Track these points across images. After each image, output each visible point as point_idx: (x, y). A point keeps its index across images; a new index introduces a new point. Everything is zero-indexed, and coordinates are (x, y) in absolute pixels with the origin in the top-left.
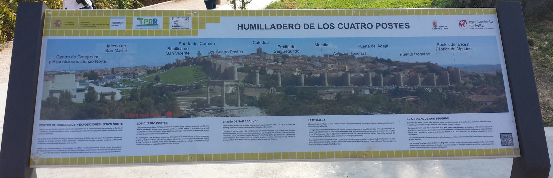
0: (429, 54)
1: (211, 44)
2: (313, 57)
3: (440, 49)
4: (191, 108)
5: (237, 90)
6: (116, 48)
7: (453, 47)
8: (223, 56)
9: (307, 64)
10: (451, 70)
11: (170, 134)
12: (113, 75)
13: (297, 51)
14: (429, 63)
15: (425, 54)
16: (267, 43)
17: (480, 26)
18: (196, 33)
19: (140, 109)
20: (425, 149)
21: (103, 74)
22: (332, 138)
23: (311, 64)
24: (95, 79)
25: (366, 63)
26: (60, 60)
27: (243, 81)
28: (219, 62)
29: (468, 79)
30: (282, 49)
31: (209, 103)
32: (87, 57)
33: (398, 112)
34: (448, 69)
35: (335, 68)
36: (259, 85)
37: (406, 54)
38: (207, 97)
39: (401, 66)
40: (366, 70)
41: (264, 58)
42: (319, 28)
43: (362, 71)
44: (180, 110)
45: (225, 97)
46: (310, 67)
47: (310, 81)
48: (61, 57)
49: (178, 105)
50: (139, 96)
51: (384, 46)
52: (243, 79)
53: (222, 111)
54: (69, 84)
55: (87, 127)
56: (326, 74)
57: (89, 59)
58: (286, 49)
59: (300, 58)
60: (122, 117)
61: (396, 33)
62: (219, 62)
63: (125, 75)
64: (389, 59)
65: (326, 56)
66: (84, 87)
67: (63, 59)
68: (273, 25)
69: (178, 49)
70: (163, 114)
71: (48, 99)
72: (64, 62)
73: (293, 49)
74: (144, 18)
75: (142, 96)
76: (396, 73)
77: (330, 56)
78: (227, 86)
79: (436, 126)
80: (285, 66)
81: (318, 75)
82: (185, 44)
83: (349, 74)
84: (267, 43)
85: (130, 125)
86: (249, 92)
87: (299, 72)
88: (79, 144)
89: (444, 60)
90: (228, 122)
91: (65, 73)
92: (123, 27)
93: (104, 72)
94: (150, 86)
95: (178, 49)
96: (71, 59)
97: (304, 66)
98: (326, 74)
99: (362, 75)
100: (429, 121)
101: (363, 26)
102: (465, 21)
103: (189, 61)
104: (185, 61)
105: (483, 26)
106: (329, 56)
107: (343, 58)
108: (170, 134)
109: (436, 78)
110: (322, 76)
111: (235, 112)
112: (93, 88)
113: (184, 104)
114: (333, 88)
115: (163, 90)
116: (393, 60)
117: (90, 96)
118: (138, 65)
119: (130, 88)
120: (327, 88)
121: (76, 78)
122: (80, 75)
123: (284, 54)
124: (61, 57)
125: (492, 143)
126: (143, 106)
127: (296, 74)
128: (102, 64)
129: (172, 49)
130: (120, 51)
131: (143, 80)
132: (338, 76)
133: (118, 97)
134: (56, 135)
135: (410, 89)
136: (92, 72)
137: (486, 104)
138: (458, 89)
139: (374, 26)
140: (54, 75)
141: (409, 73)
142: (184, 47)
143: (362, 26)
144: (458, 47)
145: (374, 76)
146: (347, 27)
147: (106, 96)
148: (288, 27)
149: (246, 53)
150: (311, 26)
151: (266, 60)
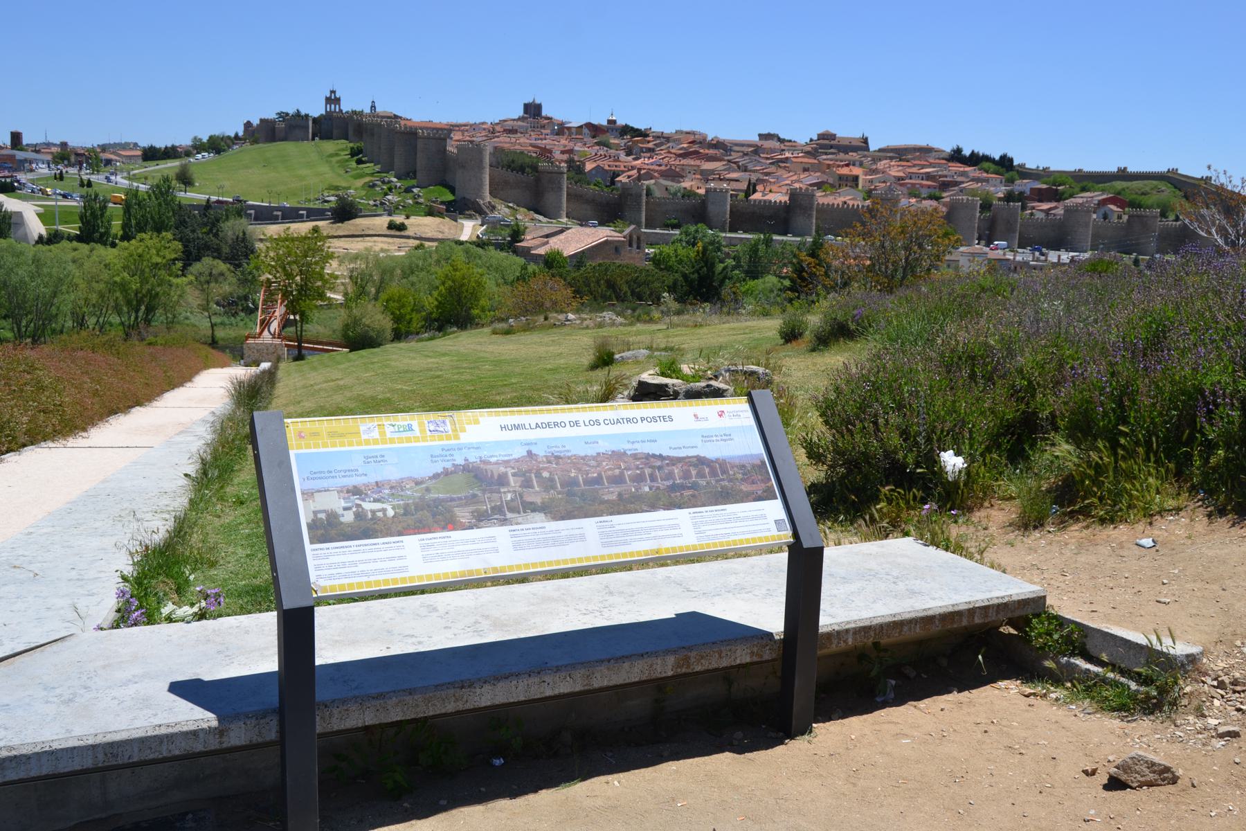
11: (457, 548)
18: (457, 437)
28: (488, 467)
33: (680, 507)
34: (717, 461)
54: (334, 503)
60: (400, 534)
62: (488, 467)
63: (392, 488)
65: (598, 454)
70: (444, 528)
75: (416, 509)
86: (529, 499)
88: (362, 567)
89: (712, 451)
92: (375, 434)
101: (629, 420)
107: (618, 456)
109: (707, 470)
110: (600, 476)
111: (520, 520)
113: (463, 515)
117: (360, 515)
125: (769, 530)
131: (412, 493)
133: (391, 513)
136: (355, 487)
138: (730, 480)
149: (516, 456)
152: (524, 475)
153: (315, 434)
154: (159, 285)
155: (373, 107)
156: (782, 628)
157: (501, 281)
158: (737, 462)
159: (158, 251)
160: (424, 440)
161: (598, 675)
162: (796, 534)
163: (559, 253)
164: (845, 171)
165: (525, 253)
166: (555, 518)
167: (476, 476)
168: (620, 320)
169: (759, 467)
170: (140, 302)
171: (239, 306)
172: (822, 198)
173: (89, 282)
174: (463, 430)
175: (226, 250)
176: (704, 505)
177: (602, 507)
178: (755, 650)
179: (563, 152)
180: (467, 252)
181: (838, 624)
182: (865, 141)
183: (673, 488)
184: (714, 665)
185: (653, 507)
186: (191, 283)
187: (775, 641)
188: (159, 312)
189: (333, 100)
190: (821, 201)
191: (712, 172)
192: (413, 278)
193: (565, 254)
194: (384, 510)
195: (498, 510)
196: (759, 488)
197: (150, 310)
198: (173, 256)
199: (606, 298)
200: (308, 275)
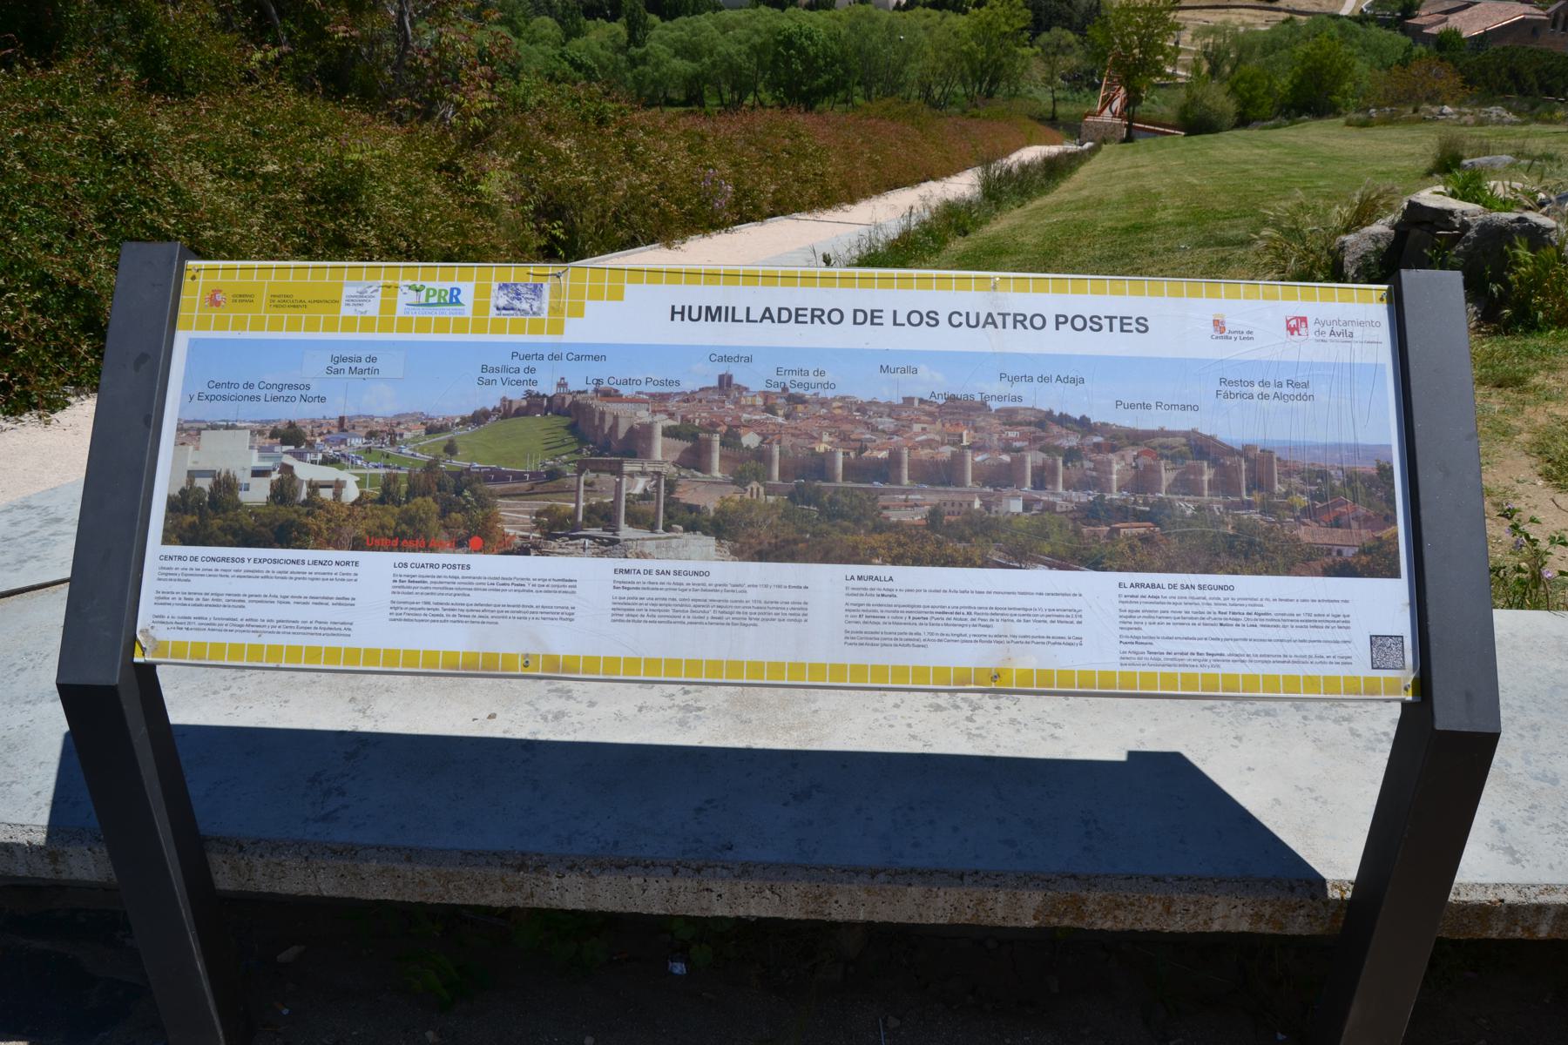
0: (1195, 408)
1: (596, 358)
2: (873, 403)
3: (1226, 396)
4: (533, 530)
5: (657, 486)
6: (353, 365)
7: (1266, 391)
8: (626, 391)
9: (853, 422)
10: (1251, 455)
11: (476, 597)
12: (343, 436)
13: (829, 386)
14: (1194, 431)
15: (1184, 408)
16: (748, 360)
17: (1344, 333)
18: (557, 328)
19: (404, 527)
20: (1158, 670)
21: (317, 431)
22: (908, 629)
23: (866, 423)
24: (297, 446)
25: (1020, 424)
26: (215, 392)
27: (674, 464)
28: (612, 408)
29: (1296, 481)
30: (787, 379)
31: (580, 518)
32: (281, 387)
33: (1096, 565)
34: (1245, 451)
35: (931, 436)
36: (717, 474)
37: (1131, 406)
38: (577, 502)
39: (1118, 439)
40: (1018, 444)
41: (736, 402)
42: (895, 324)
43: (1007, 449)
44: (504, 535)
45: (623, 504)
46: (860, 430)
47: (859, 470)
48: (218, 386)
49: (500, 521)
50: (403, 492)
51: (1073, 381)
52: (675, 456)
53: (614, 542)
54: (236, 456)
55: (272, 567)
56: (905, 451)
57: (286, 392)
58: (799, 379)
59: (835, 404)
60: (358, 545)
61: (1109, 343)
62: (612, 408)
63: (371, 435)
64: (1083, 418)
65: (908, 401)
66: (268, 464)
67: (223, 391)
68: (768, 309)
69: (508, 370)
70: (460, 544)
71: (183, 491)
72: (224, 398)
73: (819, 379)
74: (428, 285)
75: (411, 493)
76: (1099, 457)
77: (921, 401)
78: (631, 475)
79: (1195, 608)
80: (793, 424)
81: (883, 454)
82: (527, 357)
83: (969, 453)
84: (748, 360)
85: (378, 566)
86: (687, 496)
87: (831, 443)
88: (253, 611)
89: (1233, 426)
90: (628, 572)
91: (227, 428)
92: (372, 308)
93: (320, 426)
94: (431, 467)
95: (506, 369)
96: (241, 392)
97: (846, 427)
98: (905, 451)
99: (1006, 458)
100: (1178, 592)
101: (1020, 320)
102: (1304, 319)
103: (535, 404)
104: (525, 403)
105: (1351, 335)
106: (916, 403)
107: (958, 409)
108: (476, 597)
109: (1208, 475)
110: (895, 460)
111: (650, 547)
112: (290, 468)
113: (515, 517)
114: (922, 491)
115: (462, 479)
116: (1095, 418)
117: (283, 491)
118: (405, 411)
119: (383, 471)
120: (904, 492)
121: (253, 441)
122: (261, 433)
123: (792, 391)
124: (218, 386)
125: (1346, 661)
126: (410, 520)
127: (821, 448)
128: (316, 405)
129: (492, 370)
130: (362, 372)
131: (414, 451)
132: (939, 457)
133: (351, 493)
134: (198, 585)
135: (1135, 502)
136: (291, 425)
137: (1340, 553)
138: (1267, 509)
139: (1051, 322)
140: (199, 431)
141: (1135, 458)
142: (523, 364)
143: (1015, 321)
144: (1278, 390)
145: (1040, 462)
146: (973, 322)
147: (322, 491)
148: (808, 319)
149: (688, 385)
150: (873, 317)
151: (743, 408)
152: (694, 437)
153: (244, 298)
154: (1006, 55)
156: (1352, 875)
157: (1378, 64)
158: (1305, 461)
159: (1008, 19)
160: (479, 327)
161: (844, 901)
162: (1423, 684)
163: (1457, 33)
165: (1417, 33)
166: (741, 554)
167: (572, 428)
168: (1511, 117)
169: (1369, 481)
170: (985, 72)
171: (1083, 81)
173: (937, 50)
174: (578, 312)
175: (1077, 19)
176: (1170, 568)
177: (876, 540)
178: (1267, 910)
180: (1342, 28)
181: (1519, 889)
183: (1091, 513)
184: (1149, 923)
185: (1019, 557)
186: (1036, 54)
187: (1328, 902)
188: (1003, 84)
192: (1272, 57)
193: (1464, 35)
194: (338, 486)
195: (603, 516)
196: (1350, 541)
197: (994, 81)
198: (1023, 25)
199: (1504, 91)
200: (1149, 45)
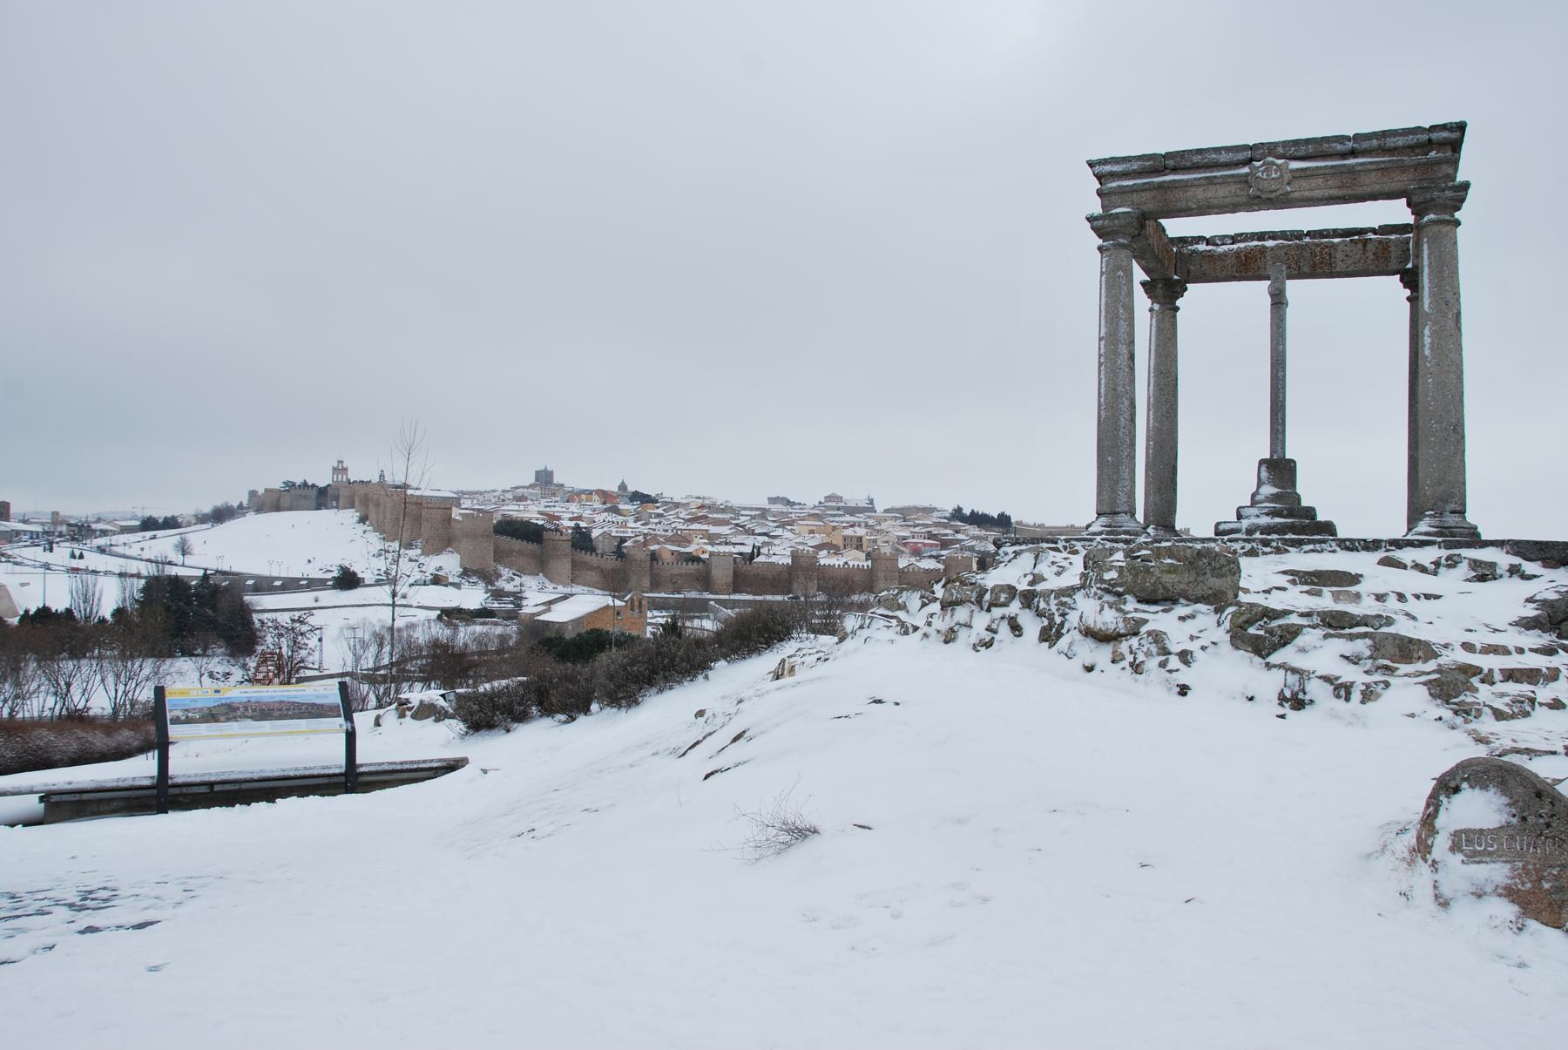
54: (179, 713)
155: (382, 476)
164: (849, 532)
172: (825, 559)
179: (571, 519)
182: (871, 502)
189: (340, 469)
190: (822, 562)
191: (719, 536)
